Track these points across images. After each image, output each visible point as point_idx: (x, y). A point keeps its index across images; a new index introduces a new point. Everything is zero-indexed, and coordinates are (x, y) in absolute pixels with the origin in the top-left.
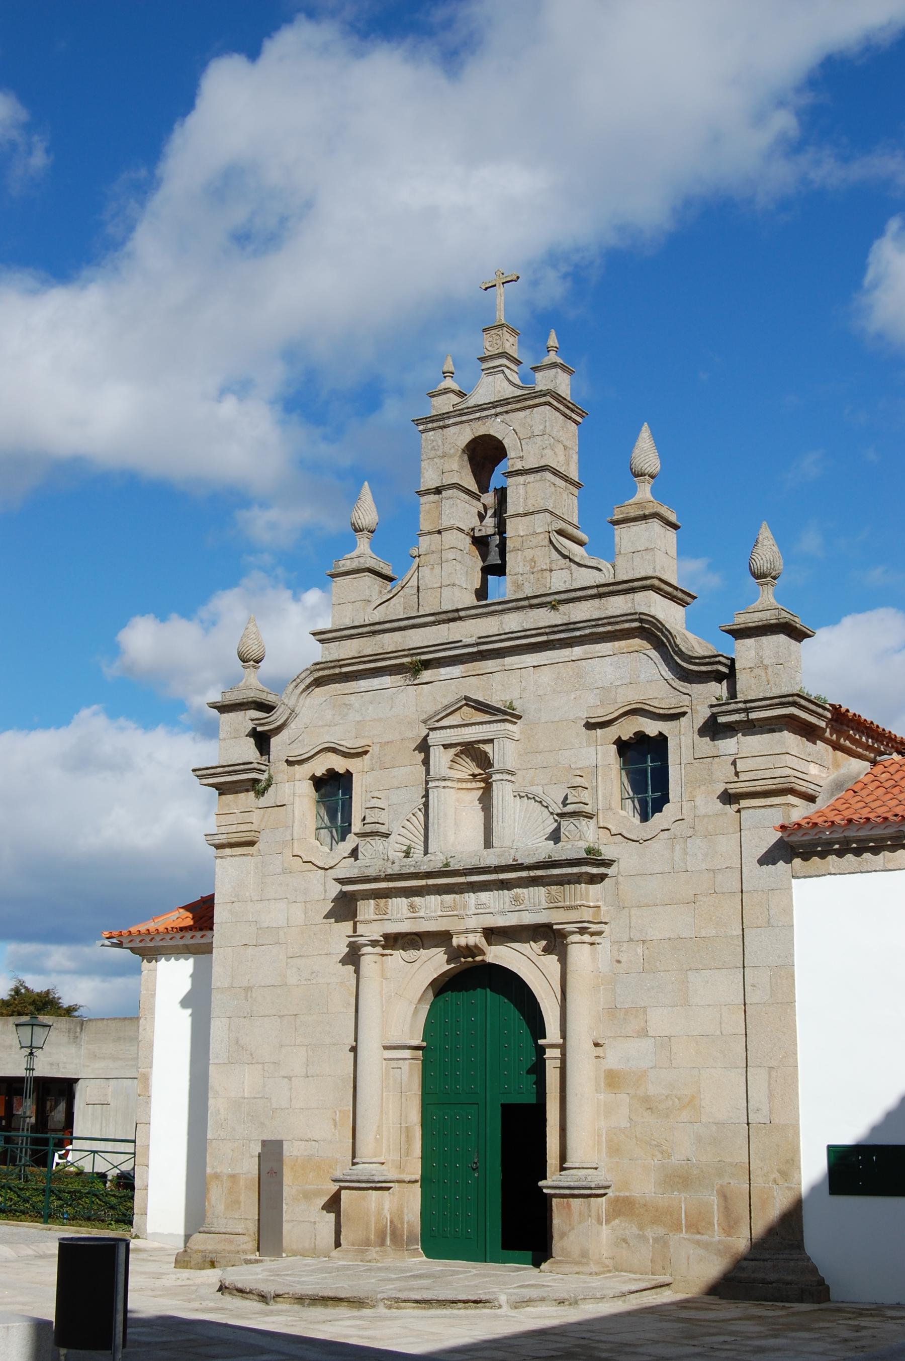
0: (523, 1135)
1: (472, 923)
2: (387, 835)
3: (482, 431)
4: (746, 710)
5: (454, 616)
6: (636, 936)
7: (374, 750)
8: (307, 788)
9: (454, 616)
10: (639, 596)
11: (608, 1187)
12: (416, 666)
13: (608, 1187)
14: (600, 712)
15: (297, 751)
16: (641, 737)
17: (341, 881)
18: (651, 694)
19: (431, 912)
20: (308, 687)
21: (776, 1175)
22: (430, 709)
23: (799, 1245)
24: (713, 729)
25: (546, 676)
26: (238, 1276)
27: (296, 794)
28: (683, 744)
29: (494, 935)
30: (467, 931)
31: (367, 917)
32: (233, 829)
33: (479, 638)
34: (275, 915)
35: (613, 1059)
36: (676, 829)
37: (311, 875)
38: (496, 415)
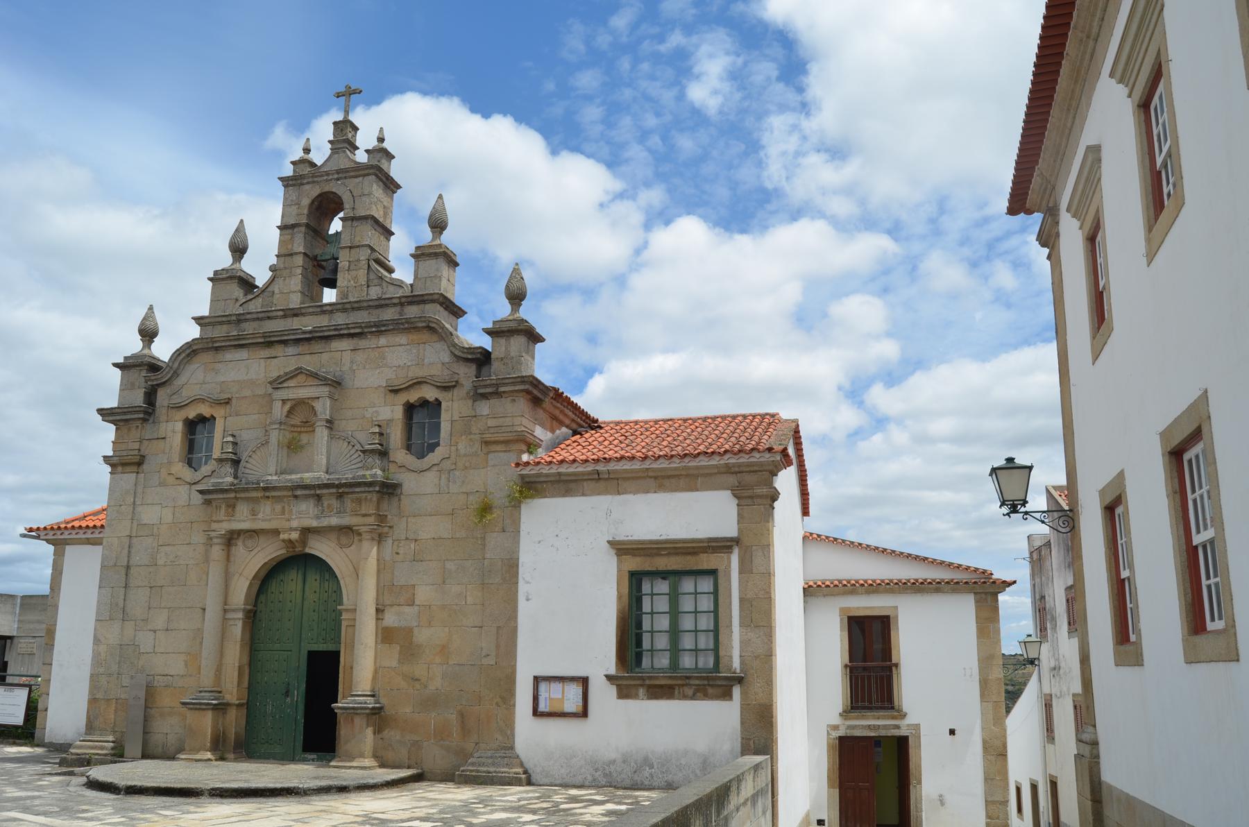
0: (324, 671)
1: (295, 524)
2: (190, 463)
3: (327, 189)
4: (497, 385)
5: (296, 313)
6: (411, 536)
7: (234, 401)
8: (179, 426)
9: (296, 313)
10: (428, 306)
11: (24, 536)
12: (269, 342)
13: (24, 536)
14: (396, 383)
15: (176, 400)
16: (424, 403)
17: (201, 492)
18: (433, 372)
19: (266, 516)
20: (188, 355)
21: (499, 700)
22: (275, 374)
23: (512, 748)
24: (479, 395)
25: (360, 356)
26: (99, 773)
27: (174, 430)
28: (453, 409)
29: (306, 532)
30: (291, 529)
31: (218, 518)
32: (125, 453)
33: (1163, 6)
34: (149, 515)
35: (390, 619)
36: (447, 465)
37: (180, 488)
38: (338, 179)
